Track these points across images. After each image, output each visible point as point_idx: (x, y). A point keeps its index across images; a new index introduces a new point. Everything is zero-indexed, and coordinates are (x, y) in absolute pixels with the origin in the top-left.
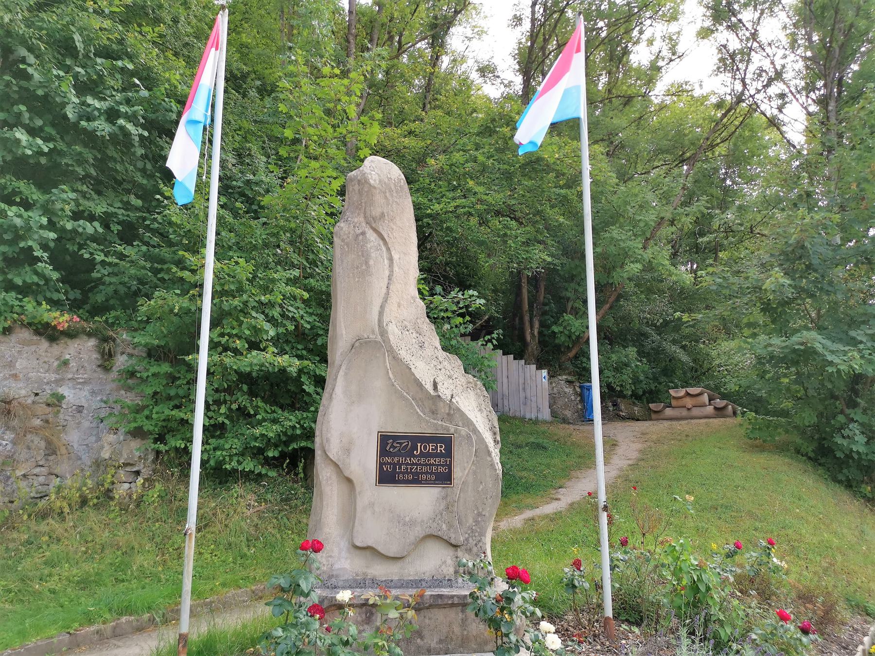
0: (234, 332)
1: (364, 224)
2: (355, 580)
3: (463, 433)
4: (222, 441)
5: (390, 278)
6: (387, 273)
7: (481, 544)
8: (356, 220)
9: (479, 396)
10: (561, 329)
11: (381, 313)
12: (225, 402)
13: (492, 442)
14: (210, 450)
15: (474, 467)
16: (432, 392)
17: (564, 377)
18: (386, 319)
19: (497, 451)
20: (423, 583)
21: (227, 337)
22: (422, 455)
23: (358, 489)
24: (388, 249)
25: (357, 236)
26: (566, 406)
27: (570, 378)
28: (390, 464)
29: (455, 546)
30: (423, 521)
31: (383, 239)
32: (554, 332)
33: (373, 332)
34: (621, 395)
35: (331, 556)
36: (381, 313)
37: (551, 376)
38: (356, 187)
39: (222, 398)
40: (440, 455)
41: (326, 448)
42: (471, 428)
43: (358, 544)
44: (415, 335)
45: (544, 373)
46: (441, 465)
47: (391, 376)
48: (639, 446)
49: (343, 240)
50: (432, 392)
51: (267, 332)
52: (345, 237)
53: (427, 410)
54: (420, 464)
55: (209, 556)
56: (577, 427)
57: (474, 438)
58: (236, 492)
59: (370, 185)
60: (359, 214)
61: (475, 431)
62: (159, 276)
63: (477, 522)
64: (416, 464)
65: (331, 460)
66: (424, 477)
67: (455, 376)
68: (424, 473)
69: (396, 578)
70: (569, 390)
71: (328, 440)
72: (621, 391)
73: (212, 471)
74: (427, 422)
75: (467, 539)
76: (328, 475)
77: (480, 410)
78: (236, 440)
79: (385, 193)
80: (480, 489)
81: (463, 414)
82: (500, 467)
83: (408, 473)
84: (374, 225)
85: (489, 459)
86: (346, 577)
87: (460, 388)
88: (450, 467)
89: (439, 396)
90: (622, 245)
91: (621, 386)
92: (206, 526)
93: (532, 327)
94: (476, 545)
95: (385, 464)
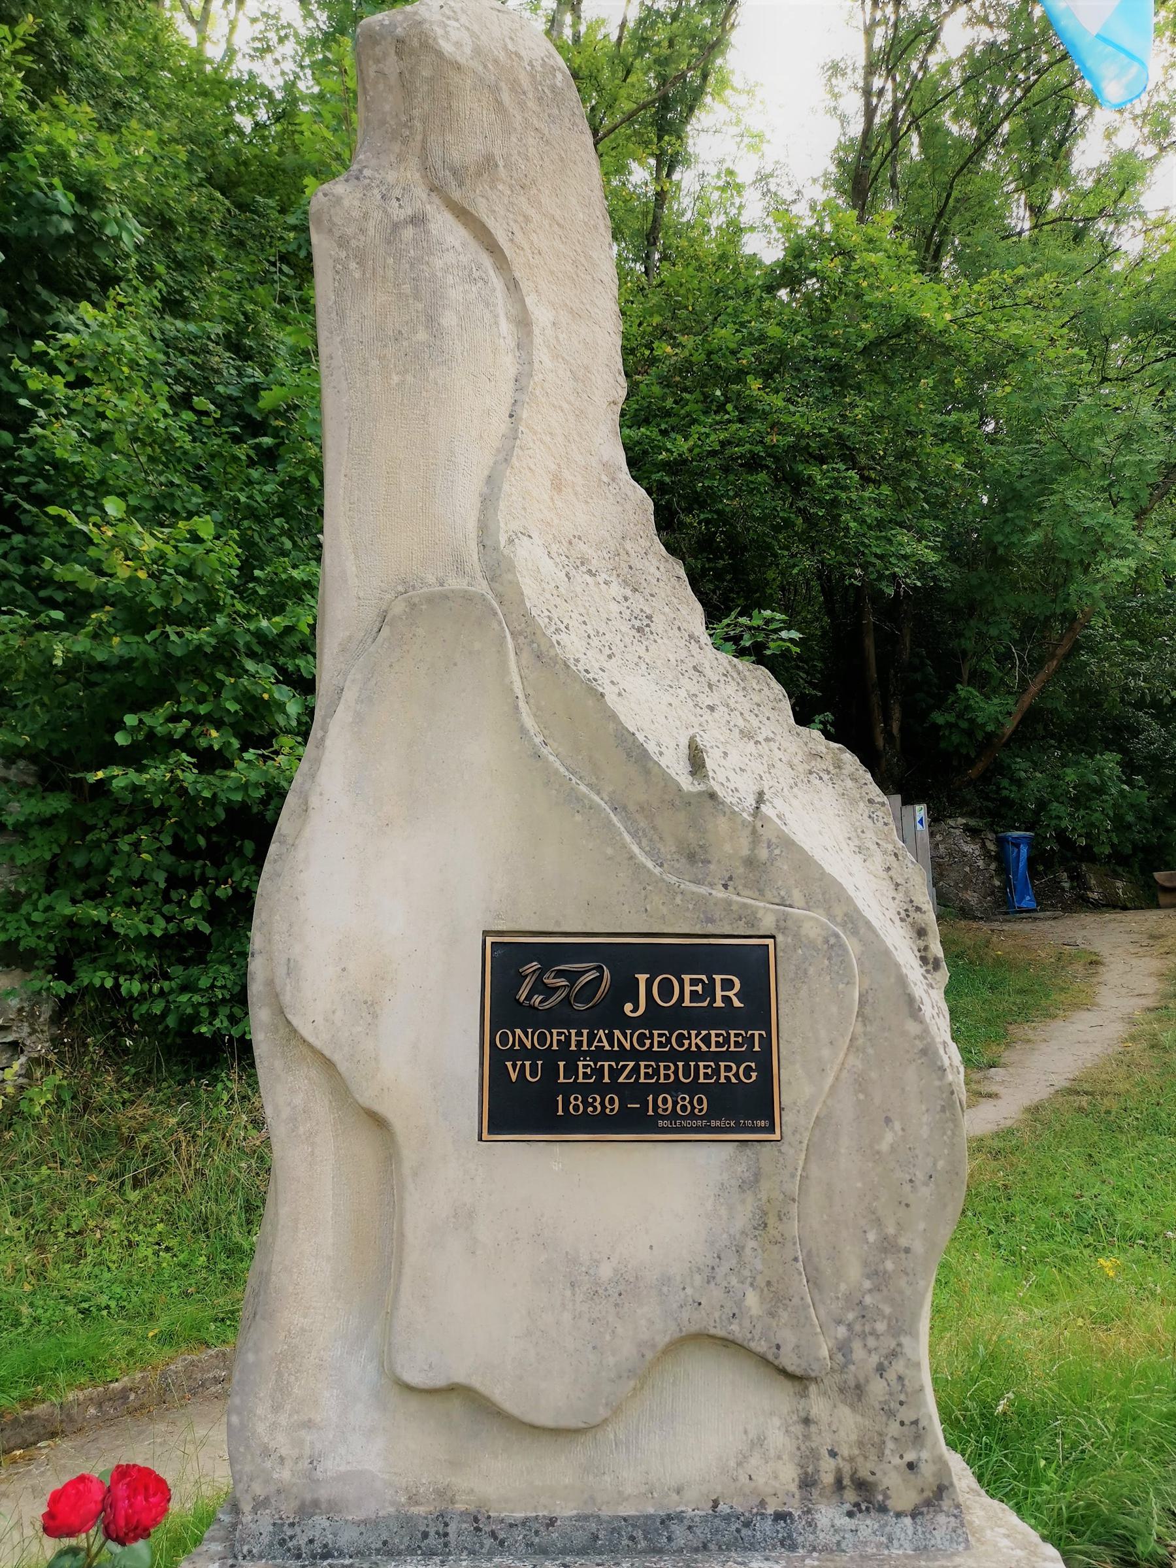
0: (203, 710)
1: (421, 192)
2: (407, 1522)
3: (811, 931)
4: (195, 971)
5: (520, 383)
6: (508, 364)
7: (899, 1366)
8: (391, 177)
9: (853, 802)
10: (951, 718)
11: (488, 502)
12: (204, 882)
13: (916, 963)
14: (172, 991)
15: (855, 1061)
16: (686, 782)
17: (961, 820)
18: (505, 525)
19: (938, 995)
20: (678, 1530)
21: (186, 723)
22: (655, 1017)
23: (409, 1156)
24: (513, 286)
25: (396, 226)
26: (967, 882)
27: (973, 823)
28: (532, 1054)
29: (799, 1380)
30: (666, 1280)
31: (492, 248)
32: (936, 727)
33: (459, 566)
34: (1088, 855)
35: (308, 1424)
36: (488, 502)
37: (936, 818)
38: (392, 65)
39: (198, 872)
40: (726, 1018)
41: (287, 999)
42: (839, 911)
43: (414, 1377)
44: (616, 589)
45: (921, 811)
46: (728, 1056)
47: (529, 722)
48: (1155, 964)
49: (343, 242)
50: (686, 782)
51: (281, 707)
52: (350, 231)
53: (668, 848)
54: (649, 1055)
55: (149, 1252)
56: (996, 925)
57: (852, 947)
58: (226, 1088)
59: (439, 54)
60: (401, 159)
61: (854, 921)
62: (42, 594)
63: (879, 1278)
64: (634, 1055)
65: (310, 1046)
66: (665, 1102)
67: (765, 732)
68: (666, 1088)
69: (566, 1510)
70: (971, 848)
71: (292, 968)
72: (1088, 847)
73: (178, 1041)
74: (672, 891)
75: (843, 1348)
76: (298, 1100)
77: (860, 850)
78: (225, 969)
79: (495, 89)
80: (884, 1146)
81: (804, 863)
82: (957, 1057)
83: (602, 1089)
84: (456, 195)
85: (912, 1028)
86: (368, 1510)
87: (784, 776)
88: (765, 1062)
89: (712, 796)
90: (1088, 521)
91: (1088, 836)
92: (152, 1173)
93: (887, 719)
94: (881, 1370)
95: (513, 1055)
